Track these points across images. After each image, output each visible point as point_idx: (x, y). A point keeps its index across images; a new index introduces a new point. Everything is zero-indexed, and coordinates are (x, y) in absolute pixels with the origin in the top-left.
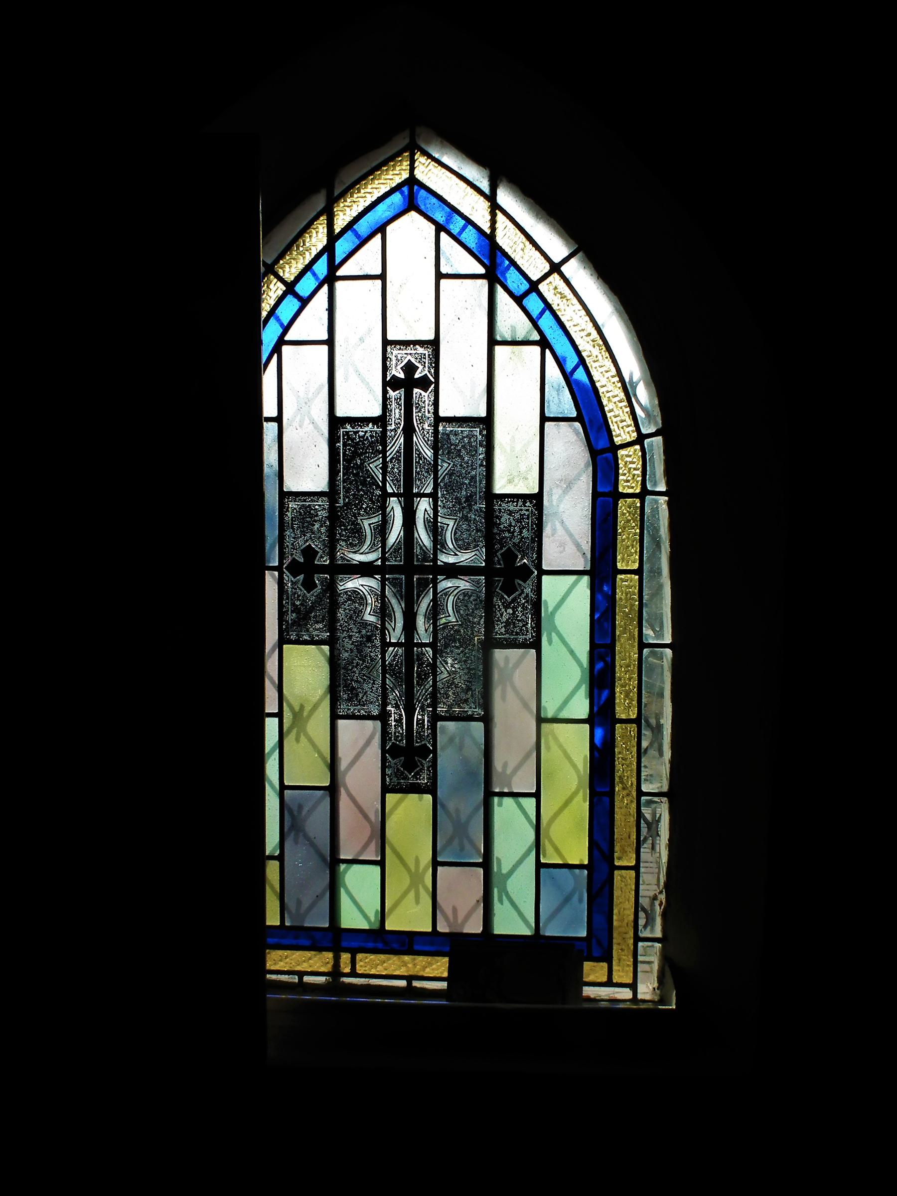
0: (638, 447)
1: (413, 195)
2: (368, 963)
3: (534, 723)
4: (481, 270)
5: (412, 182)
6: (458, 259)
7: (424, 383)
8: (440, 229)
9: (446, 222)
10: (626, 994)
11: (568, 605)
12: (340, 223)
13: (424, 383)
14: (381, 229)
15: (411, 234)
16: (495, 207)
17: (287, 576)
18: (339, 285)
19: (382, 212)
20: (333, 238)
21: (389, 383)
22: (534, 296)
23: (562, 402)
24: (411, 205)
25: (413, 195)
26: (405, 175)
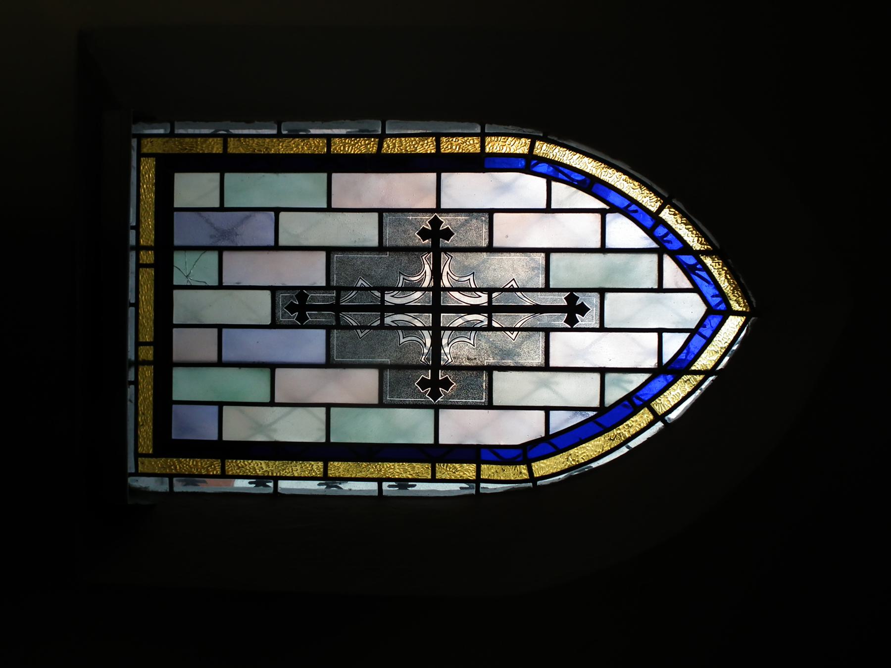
0: (526, 477)
1: (717, 312)
2: (148, 277)
3: (275, 408)
4: (666, 358)
5: (729, 312)
6: (673, 344)
7: (572, 320)
8: (693, 332)
9: (700, 334)
10: (131, 469)
11: (411, 425)
12: (708, 261)
13: (572, 320)
14: (696, 289)
15: (690, 309)
16: (707, 373)
17: (428, 217)
18: (654, 258)
19: (709, 290)
20: (696, 254)
21: (572, 294)
22: (319, 474)
23: (561, 421)
24: (711, 311)
25: (717, 312)
26: (736, 307)
